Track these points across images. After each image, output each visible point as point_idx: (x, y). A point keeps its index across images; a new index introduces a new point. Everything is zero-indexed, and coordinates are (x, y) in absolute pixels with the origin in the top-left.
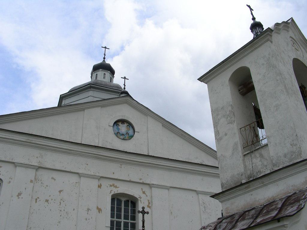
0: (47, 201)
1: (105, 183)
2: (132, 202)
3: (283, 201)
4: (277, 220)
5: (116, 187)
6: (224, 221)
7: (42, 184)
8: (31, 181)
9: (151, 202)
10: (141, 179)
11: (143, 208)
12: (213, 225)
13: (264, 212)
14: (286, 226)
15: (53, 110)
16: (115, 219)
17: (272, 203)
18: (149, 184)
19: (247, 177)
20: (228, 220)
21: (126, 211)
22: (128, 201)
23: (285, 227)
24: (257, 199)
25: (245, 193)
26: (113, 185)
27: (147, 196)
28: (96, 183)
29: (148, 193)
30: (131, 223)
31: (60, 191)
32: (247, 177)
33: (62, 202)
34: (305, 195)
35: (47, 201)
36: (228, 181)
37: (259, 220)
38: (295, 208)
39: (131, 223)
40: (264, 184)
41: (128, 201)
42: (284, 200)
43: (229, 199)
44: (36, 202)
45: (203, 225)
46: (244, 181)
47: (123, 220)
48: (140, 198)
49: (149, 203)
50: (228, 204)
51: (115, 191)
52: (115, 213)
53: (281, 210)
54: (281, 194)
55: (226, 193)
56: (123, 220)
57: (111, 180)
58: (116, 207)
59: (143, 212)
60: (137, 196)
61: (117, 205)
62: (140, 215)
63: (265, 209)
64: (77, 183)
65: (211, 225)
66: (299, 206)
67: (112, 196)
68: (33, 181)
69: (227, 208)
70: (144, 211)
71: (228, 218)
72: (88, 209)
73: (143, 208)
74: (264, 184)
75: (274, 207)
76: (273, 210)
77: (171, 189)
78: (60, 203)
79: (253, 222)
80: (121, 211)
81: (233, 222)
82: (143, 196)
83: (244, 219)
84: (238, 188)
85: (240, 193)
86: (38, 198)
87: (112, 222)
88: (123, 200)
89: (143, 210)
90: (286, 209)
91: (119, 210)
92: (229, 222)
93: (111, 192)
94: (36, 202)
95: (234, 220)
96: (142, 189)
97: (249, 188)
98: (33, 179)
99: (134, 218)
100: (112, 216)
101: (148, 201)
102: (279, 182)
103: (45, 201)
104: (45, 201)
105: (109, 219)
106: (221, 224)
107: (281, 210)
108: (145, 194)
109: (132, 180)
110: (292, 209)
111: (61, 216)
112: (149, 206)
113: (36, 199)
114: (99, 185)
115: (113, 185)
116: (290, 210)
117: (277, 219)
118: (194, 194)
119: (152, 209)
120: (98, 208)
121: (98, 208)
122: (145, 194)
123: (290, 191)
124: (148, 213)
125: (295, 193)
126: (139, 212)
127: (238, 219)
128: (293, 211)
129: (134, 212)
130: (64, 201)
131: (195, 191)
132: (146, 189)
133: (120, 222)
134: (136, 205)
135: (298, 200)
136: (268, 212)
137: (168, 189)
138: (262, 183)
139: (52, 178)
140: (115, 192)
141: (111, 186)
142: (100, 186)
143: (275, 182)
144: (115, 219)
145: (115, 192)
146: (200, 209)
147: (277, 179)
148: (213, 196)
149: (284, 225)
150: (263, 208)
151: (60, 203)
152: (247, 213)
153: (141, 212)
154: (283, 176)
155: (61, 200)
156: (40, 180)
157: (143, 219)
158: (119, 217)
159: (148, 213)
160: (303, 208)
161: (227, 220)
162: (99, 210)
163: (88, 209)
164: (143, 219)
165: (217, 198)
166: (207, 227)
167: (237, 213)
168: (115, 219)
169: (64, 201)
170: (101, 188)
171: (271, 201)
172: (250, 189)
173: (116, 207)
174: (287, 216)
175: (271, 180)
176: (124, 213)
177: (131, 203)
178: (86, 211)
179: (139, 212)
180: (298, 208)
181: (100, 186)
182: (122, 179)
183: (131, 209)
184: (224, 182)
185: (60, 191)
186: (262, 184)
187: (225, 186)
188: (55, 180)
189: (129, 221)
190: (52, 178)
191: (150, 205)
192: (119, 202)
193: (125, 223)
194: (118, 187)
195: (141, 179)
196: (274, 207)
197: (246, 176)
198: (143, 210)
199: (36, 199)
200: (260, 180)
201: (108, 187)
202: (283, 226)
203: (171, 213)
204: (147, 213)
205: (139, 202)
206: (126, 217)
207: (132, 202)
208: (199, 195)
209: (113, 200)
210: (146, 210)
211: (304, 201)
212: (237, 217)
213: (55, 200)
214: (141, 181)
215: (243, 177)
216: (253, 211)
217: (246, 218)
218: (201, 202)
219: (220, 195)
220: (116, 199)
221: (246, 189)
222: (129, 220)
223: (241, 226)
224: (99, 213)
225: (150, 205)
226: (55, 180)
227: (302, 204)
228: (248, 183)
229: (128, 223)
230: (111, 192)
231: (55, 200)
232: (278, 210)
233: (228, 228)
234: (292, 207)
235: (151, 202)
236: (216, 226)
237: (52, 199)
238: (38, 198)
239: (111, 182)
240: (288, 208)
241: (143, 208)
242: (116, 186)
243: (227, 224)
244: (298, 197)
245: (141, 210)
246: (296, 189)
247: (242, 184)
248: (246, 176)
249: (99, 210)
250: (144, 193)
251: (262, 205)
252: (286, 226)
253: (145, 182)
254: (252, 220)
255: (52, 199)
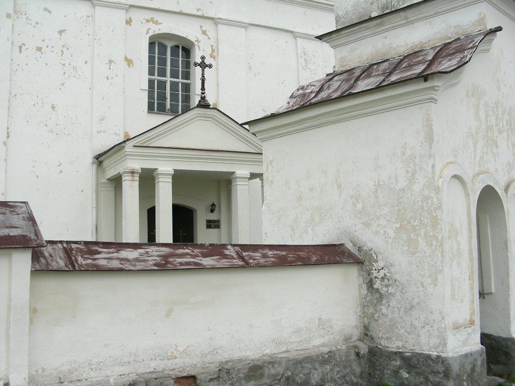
0: (39, 49)
1: (138, 17)
2: (184, 49)
3: (437, 50)
4: (423, 79)
5: (157, 23)
6: (336, 78)
7: (28, 21)
8: (9, 16)
9: (216, 50)
10: (198, 10)
11: (203, 58)
12: (318, 85)
13: (404, 66)
14: (436, 88)
15: (454, 5)
16: (156, 77)
17: (418, 52)
18: (212, 19)
19: (380, 7)
20: (344, 76)
21: (174, 64)
22: (178, 47)
23: (435, 90)
24: (395, 46)
25: (375, 34)
26: (152, 20)
27: (209, 38)
28: (121, 15)
29: (211, 34)
30: (182, 84)
31: (61, 32)
32: (380, 7)
33: (65, 50)
34: (475, 42)
35: (39, 49)
36: (347, 12)
37: (394, 78)
38: (454, 62)
39: (182, 84)
40: (409, 20)
41: (178, 47)
42: (438, 49)
43: (347, 44)
44: (20, 51)
45: (302, 84)
46: (374, 14)
47: (168, 79)
48: (198, 41)
49: (213, 51)
50: (345, 51)
51: (156, 30)
52: (156, 66)
53: (431, 62)
54: (435, 39)
55: (342, 33)
56: (168, 79)
57: (151, 11)
58: (180, 67)
59: (203, 65)
60: (193, 40)
61: (158, 54)
62: (198, 70)
63: (406, 62)
64: (88, 16)
65: (314, 84)
66: (462, 58)
67: (151, 38)
68: (12, 16)
69: (342, 58)
70: (205, 63)
71: (342, 74)
72: (111, 62)
73: (203, 58)
74: (409, 20)
75: (420, 58)
76: (419, 63)
77: (252, 27)
78: (62, 51)
79: (384, 80)
80: (165, 65)
81: (350, 80)
82: (202, 37)
83: (369, 76)
84: (363, 25)
85: (367, 34)
86: (24, 44)
87: (151, 82)
88: (169, 44)
89: (203, 62)
90: (440, 63)
91: (163, 62)
92: (344, 80)
93: (148, 32)
94: (20, 51)
95: (353, 77)
96: (201, 27)
97: (383, 26)
98: (11, 12)
99: (187, 76)
100: (151, 72)
101: (212, 46)
102: (434, 18)
103: (37, 50)
104: (37, 50)
105: (145, 77)
106: (331, 82)
107: (431, 62)
108: (206, 35)
109: (184, 11)
110: (450, 62)
111: (64, 74)
112: (212, 56)
113: (20, 47)
114: (126, 20)
115: (152, 20)
116: (446, 64)
117: (424, 77)
118: (289, 38)
119: (218, 61)
120: (126, 59)
121: (126, 59)
122: (206, 35)
123: (450, 35)
124: (210, 66)
125: (459, 39)
126: (196, 64)
127: (360, 75)
128: (451, 66)
129: (187, 65)
130: (68, 49)
131: (292, 32)
132: (208, 26)
133: (165, 82)
134: (191, 54)
135: (461, 50)
136: (410, 67)
137: (246, 28)
138: (406, 19)
139: (46, 9)
140: (154, 31)
141: (148, 21)
142: (129, 22)
143: (427, 17)
144: (156, 77)
145: (154, 31)
146: (298, 63)
147: (430, 13)
148: (315, 37)
149: (434, 87)
150: (401, 60)
151: (62, 51)
152: (375, 67)
153: (199, 65)
154: (441, 10)
155: (64, 46)
156: (23, 13)
157: (203, 76)
158: (162, 73)
159: (210, 66)
160: (467, 62)
161: (342, 77)
162: (129, 62)
163: (111, 62)
164: (203, 76)
165: (327, 40)
166: (308, 86)
167: (359, 67)
168: (156, 77)
169: (68, 49)
170: (130, 25)
171: (417, 50)
172: (383, 28)
173: (180, 67)
174: (439, 72)
175: (420, 14)
176: (171, 66)
177: (182, 50)
178: (107, 64)
179: (196, 64)
180: (459, 62)
181: (129, 22)
182: (167, 9)
183: (182, 61)
184: (340, 13)
185: (61, 32)
186: (405, 21)
187: (343, 20)
188: (50, 12)
189: (180, 80)
190: (46, 9)
191: (214, 54)
192: (163, 48)
193: (172, 83)
194: (160, 24)
195: (198, 10)
196: (420, 58)
197: (380, 5)
198: (203, 62)
199: (20, 47)
200: (402, 14)
201: (142, 23)
202: (432, 88)
203: (250, 67)
204: (210, 66)
205: (197, 47)
206: (174, 74)
207: (185, 49)
208: (298, 38)
209: (152, 44)
210: (207, 62)
211: (471, 51)
212: (357, 73)
213: (53, 47)
214: (200, 13)
215: (375, 6)
216: (386, 64)
217: (373, 74)
218: (300, 51)
219: (333, 36)
220: (157, 44)
221: (378, 27)
222: (178, 78)
223: (364, 86)
224: (129, 67)
225: (214, 54)
226: (50, 12)
227: (466, 56)
228: (381, 18)
229: (178, 83)
230: (148, 32)
231: (53, 47)
232: (427, 63)
233: (341, 89)
234: (450, 60)
235: (216, 50)
236: (323, 86)
237: (47, 47)
238: (24, 44)
239: (149, 15)
240: (443, 62)
241: (203, 58)
242: (157, 20)
243: (342, 83)
244: (461, 46)
245: (199, 61)
246: (460, 32)
247: (371, 19)
248: (380, 5)
249: (129, 62)
250: (204, 33)
251: (400, 56)
252: (436, 88)
253: (206, 15)
254: (382, 78)
255: (47, 47)
